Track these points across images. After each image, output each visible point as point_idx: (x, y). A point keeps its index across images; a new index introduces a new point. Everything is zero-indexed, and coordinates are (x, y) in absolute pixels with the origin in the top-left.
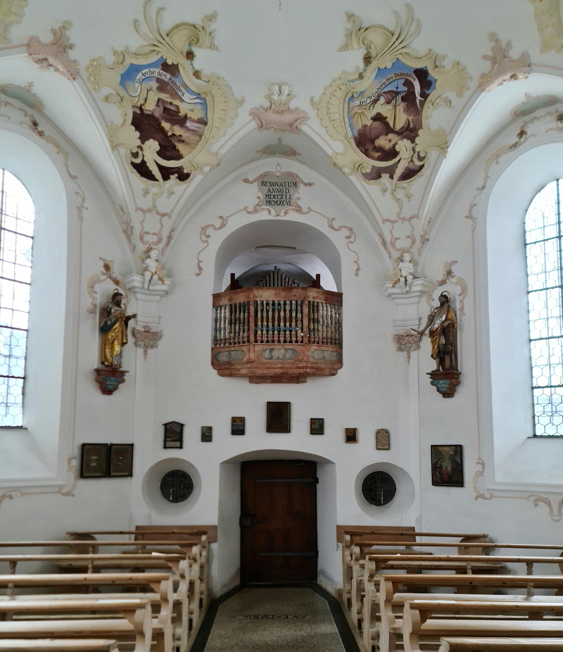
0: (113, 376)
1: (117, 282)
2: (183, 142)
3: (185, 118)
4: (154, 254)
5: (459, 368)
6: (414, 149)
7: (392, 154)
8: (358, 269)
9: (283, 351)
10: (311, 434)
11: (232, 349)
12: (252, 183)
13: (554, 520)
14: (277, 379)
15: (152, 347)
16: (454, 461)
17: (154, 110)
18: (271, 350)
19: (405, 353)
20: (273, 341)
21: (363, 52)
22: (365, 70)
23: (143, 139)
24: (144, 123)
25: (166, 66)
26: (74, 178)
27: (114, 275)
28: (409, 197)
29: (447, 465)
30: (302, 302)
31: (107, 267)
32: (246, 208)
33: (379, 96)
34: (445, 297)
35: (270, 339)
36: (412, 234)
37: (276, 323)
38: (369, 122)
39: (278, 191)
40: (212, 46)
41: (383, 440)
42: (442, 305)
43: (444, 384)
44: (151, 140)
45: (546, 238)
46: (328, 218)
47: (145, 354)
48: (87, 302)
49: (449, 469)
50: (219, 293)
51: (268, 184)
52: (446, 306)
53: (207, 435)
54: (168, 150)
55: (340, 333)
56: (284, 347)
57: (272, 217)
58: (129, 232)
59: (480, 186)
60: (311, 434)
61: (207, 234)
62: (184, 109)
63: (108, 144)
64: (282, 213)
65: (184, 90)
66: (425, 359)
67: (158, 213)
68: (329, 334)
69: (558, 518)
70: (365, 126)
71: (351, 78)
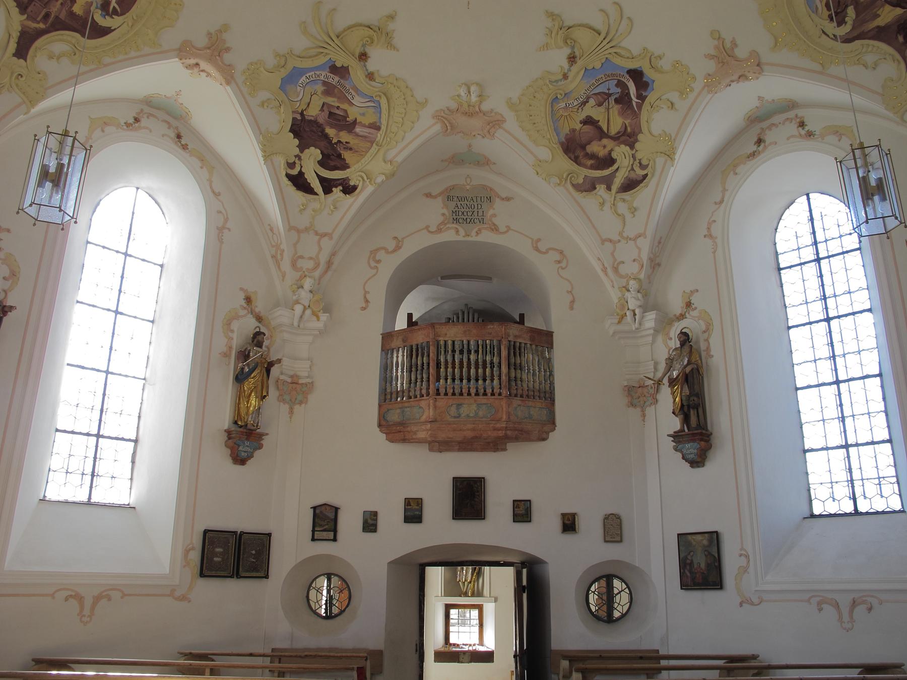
0: (247, 439)
1: (259, 319)
2: (351, 149)
3: (355, 122)
4: (308, 283)
5: (709, 428)
6: (634, 156)
7: (608, 161)
8: (573, 302)
9: (474, 407)
10: (514, 521)
11: (406, 405)
12: (435, 197)
13: (845, 629)
14: (467, 445)
15: (301, 403)
16: (709, 554)
17: (317, 116)
18: (459, 406)
19: (639, 409)
20: (461, 394)
21: (567, 51)
22: (569, 70)
23: (302, 147)
24: (304, 130)
25: (334, 69)
26: (217, 195)
27: (257, 310)
28: (633, 211)
29: (700, 561)
30: (500, 342)
31: (248, 300)
32: (427, 227)
33: (588, 98)
34: (686, 334)
35: (456, 391)
36: (639, 256)
37: (465, 370)
38: (578, 126)
39: (468, 207)
40: (390, 45)
41: (613, 529)
42: (683, 344)
43: (691, 448)
44: (312, 148)
45: (802, 261)
46: (532, 240)
47: (291, 412)
48: (220, 343)
49: (703, 566)
50: (390, 333)
51: (455, 199)
52: (686, 348)
53: (370, 524)
54: (332, 158)
55: (552, 384)
56: (475, 401)
57: (460, 238)
58: (279, 257)
59: (718, 200)
60: (514, 521)
61: (377, 258)
62: (353, 113)
63: (260, 153)
64: (474, 233)
65: (353, 93)
66: (665, 416)
67: (316, 233)
68: (537, 385)
69: (850, 626)
70: (574, 130)
71: (553, 78)
